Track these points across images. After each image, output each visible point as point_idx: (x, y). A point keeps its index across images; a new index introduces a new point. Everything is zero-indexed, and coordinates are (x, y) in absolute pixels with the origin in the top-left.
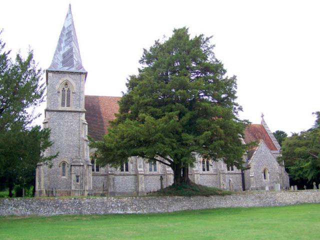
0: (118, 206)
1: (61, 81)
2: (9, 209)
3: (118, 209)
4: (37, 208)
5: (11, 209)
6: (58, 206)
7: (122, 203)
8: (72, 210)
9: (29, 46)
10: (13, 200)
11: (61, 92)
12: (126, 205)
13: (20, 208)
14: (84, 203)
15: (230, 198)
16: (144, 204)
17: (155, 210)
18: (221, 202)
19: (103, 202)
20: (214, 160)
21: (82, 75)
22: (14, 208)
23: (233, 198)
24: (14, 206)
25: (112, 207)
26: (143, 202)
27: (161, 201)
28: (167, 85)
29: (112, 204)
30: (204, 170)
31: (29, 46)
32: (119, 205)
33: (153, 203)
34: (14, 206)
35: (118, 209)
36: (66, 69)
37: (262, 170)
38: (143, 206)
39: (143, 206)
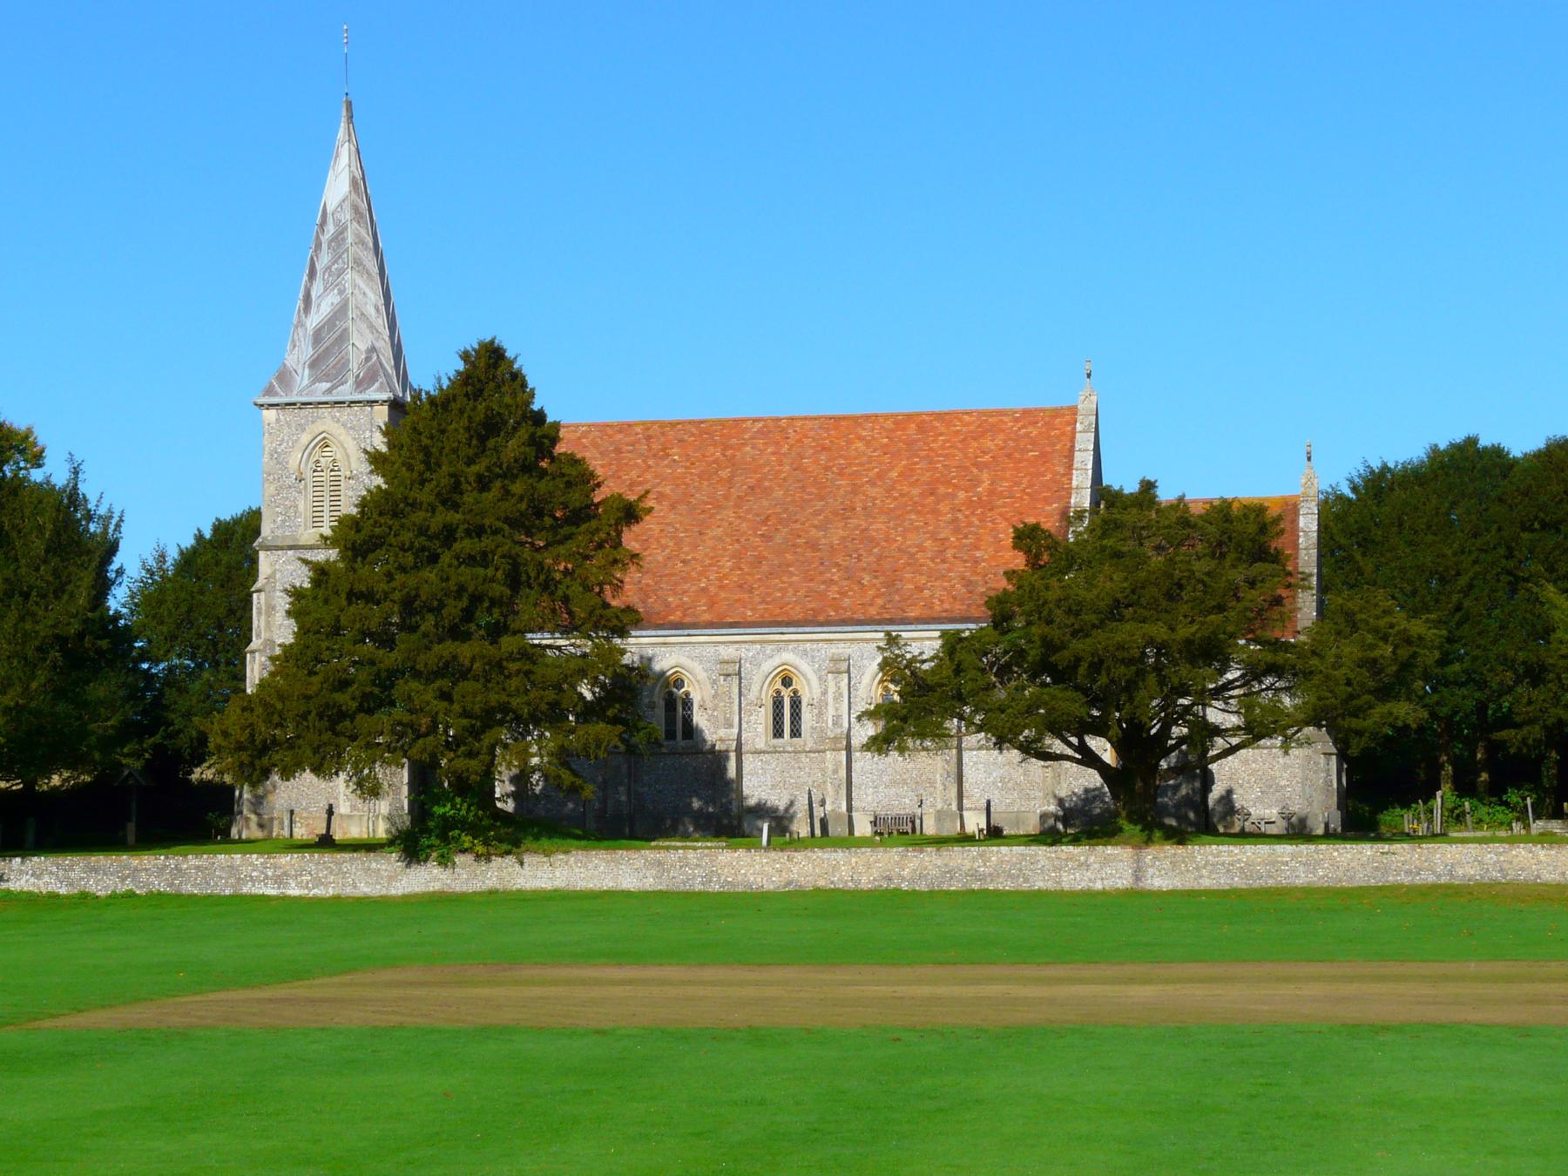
0: (267, 877)
1: (305, 438)
2: (23, 882)
3: (266, 884)
4: (83, 878)
5: (27, 881)
6: (128, 877)
7: (275, 867)
8: (159, 885)
9: (70, 454)
10: (31, 861)
11: (308, 475)
12: (285, 874)
13: (46, 878)
14: (187, 869)
15: (567, 863)
16: (331, 873)
17: (355, 887)
18: (539, 874)
19: (231, 867)
20: (1057, 665)
21: (377, 408)
22: (32, 880)
23: (576, 863)
24: (32, 876)
25: (251, 876)
26: (327, 868)
27: (374, 865)
28: (485, 495)
29: (254, 870)
30: (778, 733)
31: (70, 454)
32: (270, 874)
33: (354, 870)
34: (32, 876)
35: (266, 884)
36: (320, 391)
37: (324, 805)
38: (326, 877)
39: (326, 877)
